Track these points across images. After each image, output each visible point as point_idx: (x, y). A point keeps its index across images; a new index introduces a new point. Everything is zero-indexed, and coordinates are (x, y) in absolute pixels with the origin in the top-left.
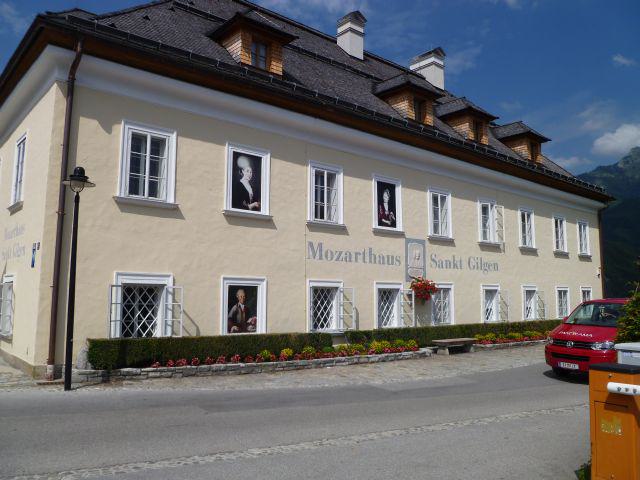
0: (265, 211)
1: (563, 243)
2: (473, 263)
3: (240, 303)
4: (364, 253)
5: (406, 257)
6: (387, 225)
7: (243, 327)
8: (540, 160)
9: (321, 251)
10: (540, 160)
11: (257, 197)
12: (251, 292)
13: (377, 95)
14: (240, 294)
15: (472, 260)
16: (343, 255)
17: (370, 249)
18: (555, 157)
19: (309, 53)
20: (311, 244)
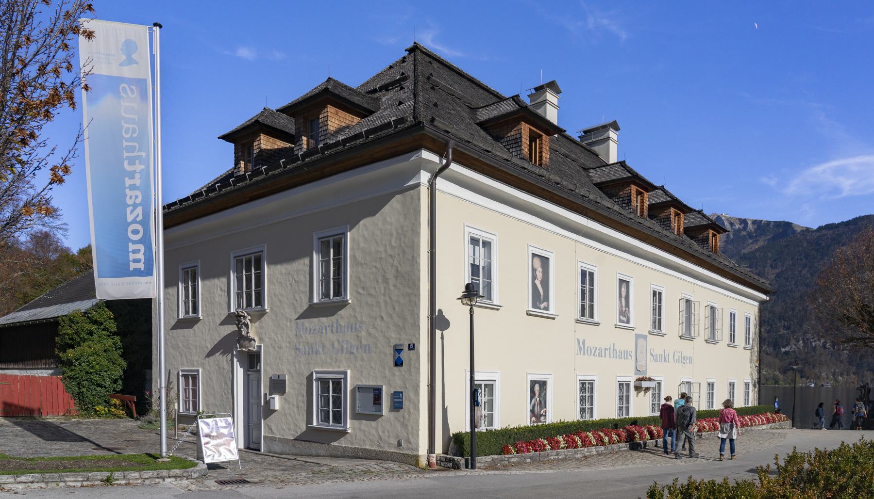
0: (552, 311)
1: (748, 330)
2: (676, 357)
3: (536, 397)
4: (610, 349)
5: (636, 352)
6: (623, 322)
7: (538, 420)
8: (441, 332)
9: (584, 346)
10: (441, 332)
11: (546, 298)
12: (543, 384)
13: (482, 125)
14: (537, 387)
15: (676, 353)
16: (597, 351)
17: (614, 344)
18: (453, 441)
19: (666, 194)
20: (578, 340)
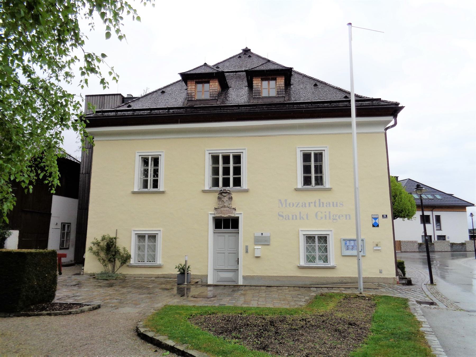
4: (315, 203)
